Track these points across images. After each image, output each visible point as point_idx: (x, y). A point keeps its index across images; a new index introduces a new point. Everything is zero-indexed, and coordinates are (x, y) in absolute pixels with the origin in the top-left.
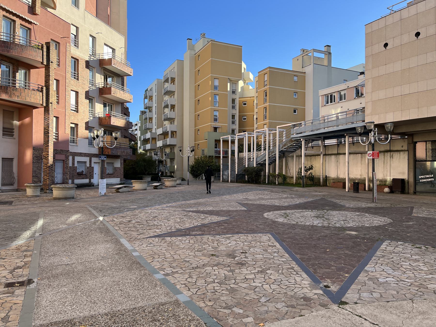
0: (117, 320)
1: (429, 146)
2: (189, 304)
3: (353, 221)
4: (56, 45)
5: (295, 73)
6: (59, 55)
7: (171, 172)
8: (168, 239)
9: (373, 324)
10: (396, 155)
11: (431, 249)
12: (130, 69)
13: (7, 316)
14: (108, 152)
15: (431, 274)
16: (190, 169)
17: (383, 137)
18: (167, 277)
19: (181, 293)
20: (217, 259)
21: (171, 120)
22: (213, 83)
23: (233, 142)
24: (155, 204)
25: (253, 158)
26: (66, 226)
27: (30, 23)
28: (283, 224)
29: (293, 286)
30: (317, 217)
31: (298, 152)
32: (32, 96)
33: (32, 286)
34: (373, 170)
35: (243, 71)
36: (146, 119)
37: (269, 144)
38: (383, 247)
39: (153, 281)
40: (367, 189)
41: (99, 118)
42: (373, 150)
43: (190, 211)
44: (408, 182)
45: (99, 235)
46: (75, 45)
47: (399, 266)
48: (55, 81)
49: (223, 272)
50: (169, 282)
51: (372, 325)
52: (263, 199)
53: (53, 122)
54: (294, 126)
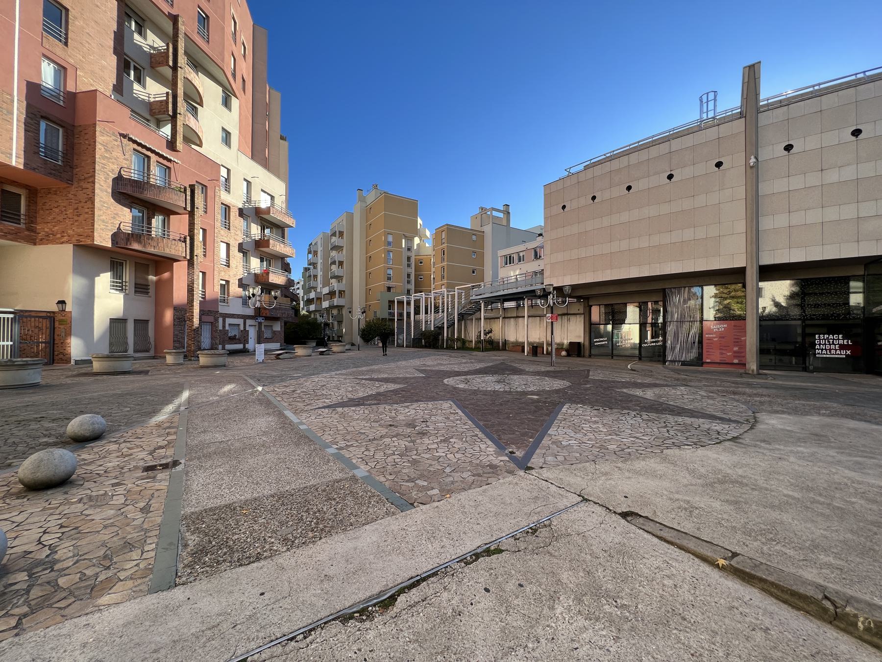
0: (286, 501)
1: (603, 309)
2: (368, 479)
3: (534, 385)
4: (203, 188)
5: (473, 232)
6: (206, 201)
7: (339, 337)
8: (340, 410)
9: (559, 487)
10: (572, 318)
11: (608, 411)
12: (292, 220)
13: (148, 505)
14: (266, 314)
15: (610, 435)
16: (360, 333)
17: (560, 300)
18: (340, 451)
19: (357, 468)
20: (396, 429)
21: (339, 278)
22: (386, 238)
23: (409, 303)
24: (322, 371)
25: (431, 321)
26: (217, 397)
27: (169, 160)
28: (464, 390)
29: (478, 454)
30: (499, 382)
31: (477, 314)
32: (173, 247)
33: (179, 468)
34: (552, 334)
35: (419, 227)
36: (310, 276)
37: (448, 306)
38: (564, 409)
39: (325, 456)
40: (545, 353)
41: (255, 274)
42: (552, 313)
43: (362, 379)
44: (584, 345)
45: (258, 407)
46: (226, 190)
47: (580, 428)
48: (201, 230)
49: (403, 443)
50: (343, 456)
51: (558, 488)
52: (442, 365)
53: (198, 279)
54: (473, 287)
